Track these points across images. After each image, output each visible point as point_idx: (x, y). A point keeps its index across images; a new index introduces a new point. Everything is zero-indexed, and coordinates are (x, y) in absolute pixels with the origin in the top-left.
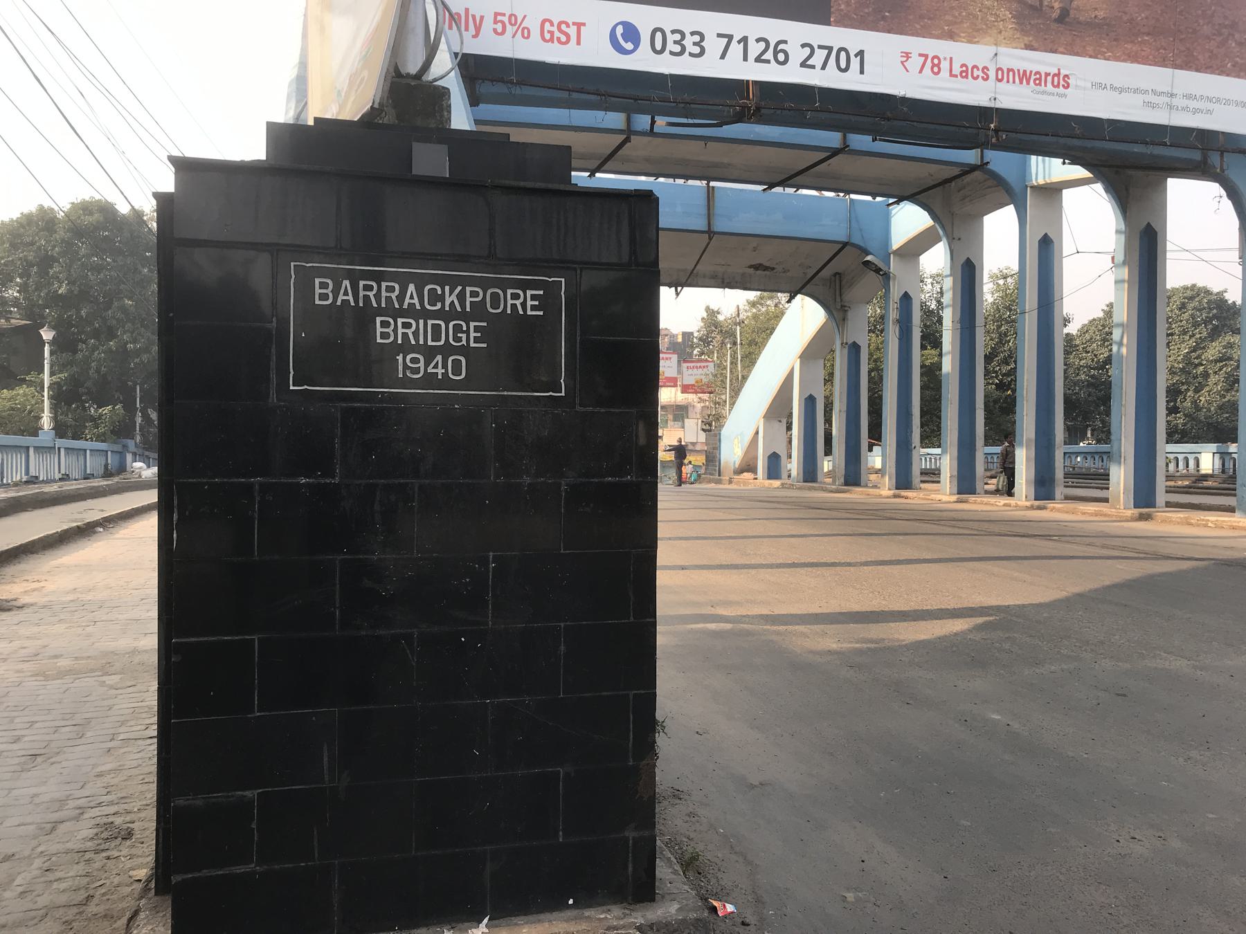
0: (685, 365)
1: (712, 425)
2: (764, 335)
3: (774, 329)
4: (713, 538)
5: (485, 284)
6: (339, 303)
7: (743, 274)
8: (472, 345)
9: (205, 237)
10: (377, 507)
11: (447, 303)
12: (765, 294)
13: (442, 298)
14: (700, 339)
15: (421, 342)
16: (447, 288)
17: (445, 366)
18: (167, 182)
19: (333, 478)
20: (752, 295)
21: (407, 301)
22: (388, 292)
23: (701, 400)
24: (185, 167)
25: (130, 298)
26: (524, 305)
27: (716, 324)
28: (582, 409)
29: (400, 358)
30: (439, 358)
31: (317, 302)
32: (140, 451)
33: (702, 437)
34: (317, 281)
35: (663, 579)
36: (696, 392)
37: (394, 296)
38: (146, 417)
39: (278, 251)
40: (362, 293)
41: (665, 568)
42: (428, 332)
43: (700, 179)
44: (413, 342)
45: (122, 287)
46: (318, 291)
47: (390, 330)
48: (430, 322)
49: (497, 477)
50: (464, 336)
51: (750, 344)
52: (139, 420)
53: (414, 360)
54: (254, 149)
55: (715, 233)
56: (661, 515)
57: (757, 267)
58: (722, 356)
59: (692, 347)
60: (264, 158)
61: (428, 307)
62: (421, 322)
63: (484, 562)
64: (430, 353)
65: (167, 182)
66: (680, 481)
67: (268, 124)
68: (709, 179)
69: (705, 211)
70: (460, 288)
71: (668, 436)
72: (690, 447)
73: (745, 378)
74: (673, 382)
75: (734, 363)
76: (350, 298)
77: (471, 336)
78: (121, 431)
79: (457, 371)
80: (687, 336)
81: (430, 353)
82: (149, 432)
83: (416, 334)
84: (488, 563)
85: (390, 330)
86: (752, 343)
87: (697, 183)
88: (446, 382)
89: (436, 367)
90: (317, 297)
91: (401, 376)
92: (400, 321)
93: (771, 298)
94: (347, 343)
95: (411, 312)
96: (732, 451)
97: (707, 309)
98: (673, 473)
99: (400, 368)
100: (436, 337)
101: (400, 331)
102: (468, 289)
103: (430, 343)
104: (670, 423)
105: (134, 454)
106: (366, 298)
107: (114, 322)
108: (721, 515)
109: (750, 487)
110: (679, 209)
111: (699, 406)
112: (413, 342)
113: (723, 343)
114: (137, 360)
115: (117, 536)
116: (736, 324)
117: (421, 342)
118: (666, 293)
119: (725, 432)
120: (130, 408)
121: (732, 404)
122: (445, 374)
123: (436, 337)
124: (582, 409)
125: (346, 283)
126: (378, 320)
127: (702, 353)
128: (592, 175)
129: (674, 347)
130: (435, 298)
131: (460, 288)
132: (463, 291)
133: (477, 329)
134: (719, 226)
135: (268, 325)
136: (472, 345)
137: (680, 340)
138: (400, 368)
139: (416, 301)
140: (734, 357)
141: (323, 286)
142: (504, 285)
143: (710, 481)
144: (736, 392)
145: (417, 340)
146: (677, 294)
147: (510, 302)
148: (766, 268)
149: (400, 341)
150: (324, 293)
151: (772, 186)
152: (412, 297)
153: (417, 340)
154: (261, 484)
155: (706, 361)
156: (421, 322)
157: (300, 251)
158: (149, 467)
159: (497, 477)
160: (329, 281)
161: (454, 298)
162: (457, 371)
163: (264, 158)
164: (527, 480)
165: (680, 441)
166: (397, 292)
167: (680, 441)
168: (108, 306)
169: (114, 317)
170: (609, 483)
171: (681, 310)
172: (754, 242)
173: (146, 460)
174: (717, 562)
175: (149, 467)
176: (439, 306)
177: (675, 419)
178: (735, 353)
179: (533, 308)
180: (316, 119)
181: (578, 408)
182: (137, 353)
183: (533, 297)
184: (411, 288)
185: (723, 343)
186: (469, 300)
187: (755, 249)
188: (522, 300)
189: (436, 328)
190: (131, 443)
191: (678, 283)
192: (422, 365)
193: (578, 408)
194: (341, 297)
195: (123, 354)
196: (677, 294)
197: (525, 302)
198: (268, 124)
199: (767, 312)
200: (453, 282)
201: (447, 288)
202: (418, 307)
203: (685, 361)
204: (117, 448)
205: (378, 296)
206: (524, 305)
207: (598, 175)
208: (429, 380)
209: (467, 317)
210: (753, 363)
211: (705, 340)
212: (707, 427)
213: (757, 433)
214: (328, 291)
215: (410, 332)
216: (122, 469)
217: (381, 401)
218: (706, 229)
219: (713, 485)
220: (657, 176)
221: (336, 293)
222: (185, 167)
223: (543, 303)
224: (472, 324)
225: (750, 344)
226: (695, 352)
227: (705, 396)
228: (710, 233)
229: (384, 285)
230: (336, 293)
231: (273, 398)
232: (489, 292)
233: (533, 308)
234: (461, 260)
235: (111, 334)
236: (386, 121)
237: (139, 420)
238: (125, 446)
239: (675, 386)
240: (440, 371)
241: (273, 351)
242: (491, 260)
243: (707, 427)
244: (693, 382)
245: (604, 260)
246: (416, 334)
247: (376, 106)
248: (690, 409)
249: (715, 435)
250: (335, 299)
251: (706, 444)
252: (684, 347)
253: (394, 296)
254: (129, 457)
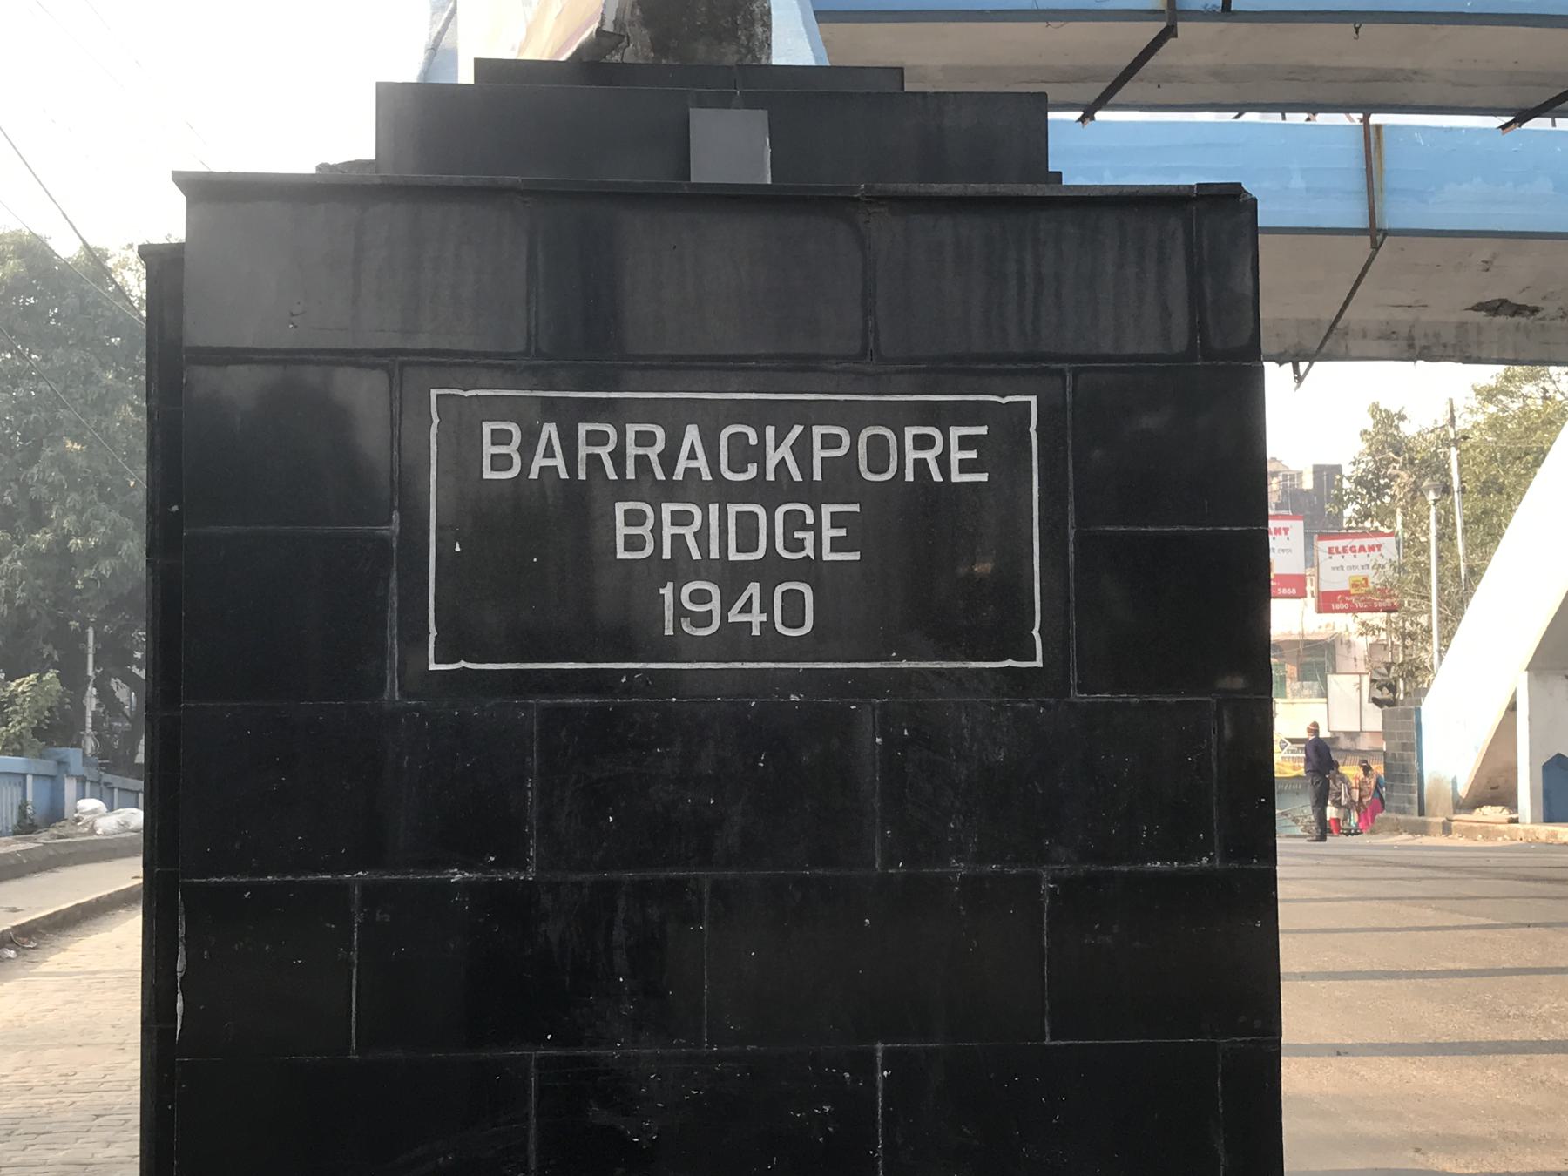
0: (1323, 545)
1: (1399, 689)
2: (1518, 468)
3: (1540, 456)
4: (1411, 975)
5: (853, 418)
6: (534, 475)
7: (1462, 325)
8: (828, 556)
9: (248, 343)
10: (619, 935)
11: (772, 461)
12: (1518, 369)
13: (759, 454)
14: (1360, 482)
15: (714, 555)
16: (770, 431)
17: (766, 607)
18: (169, 222)
19: (523, 869)
20: (1488, 374)
21: (683, 463)
22: (642, 443)
23: (1367, 629)
24: (205, 191)
25: (76, 439)
26: (944, 460)
27: (1398, 445)
28: (1085, 698)
29: (667, 592)
30: (754, 589)
31: (488, 474)
32: (93, 774)
33: (1374, 719)
34: (487, 428)
35: (1297, 1078)
36: (1353, 610)
37: (653, 453)
38: (106, 695)
39: (398, 364)
40: (583, 451)
41: (1285, 932)
42: (729, 524)
43: (1346, 108)
44: (696, 556)
45: (61, 413)
46: (489, 450)
47: (645, 531)
48: (733, 509)
49: (890, 861)
50: (808, 537)
51: (1485, 490)
52: (91, 703)
53: (700, 597)
54: (353, 139)
55: (1386, 233)
56: (1287, 916)
57: (1495, 308)
58: (1415, 522)
59: (1340, 501)
60: (369, 153)
61: (729, 475)
62: (714, 509)
63: (864, 1065)
64: (732, 579)
65: (169, 222)
66: (1324, 830)
67: (378, 84)
68: (1367, 109)
69: (1359, 183)
70: (798, 429)
71: (1293, 717)
72: (1344, 743)
73: (1475, 573)
74: (1297, 586)
75: (1446, 537)
76: (559, 462)
77: (826, 535)
78: (55, 730)
79: (793, 619)
80: (1326, 474)
81: (732, 579)
82: (111, 730)
83: (702, 536)
84: (873, 1072)
85: (645, 531)
86: (1491, 487)
87: (1340, 119)
88: (770, 644)
89: (747, 608)
90: (487, 462)
91: (669, 632)
92: (667, 509)
93: (1531, 378)
94: (544, 553)
95: (691, 488)
96: (1450, 754)
97: (1375, 409)
98: (1306, 810)
99: (669, 614)
100: (747, 544)
101: (668, 531)
102: (818, 431)
103: (733, 556)
104: (1292, 685)
105: (82, 780)
106: (594, 460)
107: (44, 490)
108: (1429, 916)
109: (1499, 842)
110: (1297, 183)
111: (1362, 644)
112: (696, 556)
113: (1416, 491)
114: (89, 573)
115: (44, 968)
116: (1447, 443)
117: (714, 555)
118: (1276, 376)
119: (1430, 709)
120: (73, 679)
121: (1447, 637)
122: (768, 626)
123: (747, 544)
124: (1085, 698)
125: (550, 430)
126: (620, 508)
127: (1365, 515)
128: (1088, 115)
129: (1297, 502)
130: (744, 454)
131: (798, 429)
132: (806, 438)
133: (837, 521)
134: (1396, 215)
135: (383, 531)
136: (828, 556)
137: (1308, 483)
138: (669, 614)
139: (701, 463)
140: (1445, 522)
141: (501, 437)
142: (897, 418)
143: (1397, 829)
144: (1454, 609)
145: (704, 547)
146: (1299, 379)
147: (912, 455)
148: (1518, 310)
149: (667, 555)
150: (503, 455)
151: (1522, 116)
152: (692, 455)
153: (704, 547)
154: (365, 886)
155: (1376, 533)
156: (714, 509)
157: (446, 362)
158: (111, 809)
159: (890, 861)
160: (513, 428)
161: (785, 451)
162: (793, 619)
163: (369, 153)
164: (959, 868)
165: (1314, 729)
166: (660, 445)
167: (1314, 729)
168: (33, 457)
169: (43, 482)
170: (1157, 874)
171: (1313, 418)
172: (1485, 249)
173: (105, 792)
174: (1424, 1037)
175: (111, 809)
176: (753, 470)
177: (1303, 676)
178: (1449, 512)
179: (965, 466)
180: (480, 64)
181: (1076, 696)
182: (91, 557)
183: (965, 443)
184: (692, 434)
185: (1416, 491)
186: (819, 454)
187: (1487, 266)
188: (938, 449)
189: (747, 524)
190: (74, 756)
191: (1296, 356)
192: (715, 605)
193: (1076, 696)
194: (539, 462)
195: (62, 560)
196: (1299, 379)
197: (948, 454)
198: (378, 84)
199: (1525, 413)
200: (781, 417)
201: (770, 431)
202: (706, 476)
203: (1322, 537)
204: (47, 766)
205: (618, 457)
206: (944, 460)
207: (1100, 115)
208: (733, 640)
209: (814, 495)
210: (1495, 535)
211: (1372, 485)
212: (1385, 694)
213: (1512, 707)
214: (512, 449)
215: (688, 533)
216: (55, 814)
217: (628, 690)
218: (1363, 223)
219: (1404, 839)
220: (1241, 108)
221: (527, 450)
222: (205, 191)
223: (986, 453)
224: (827, 510)
225: (1485, 490)
226: (1348, 513)
227: (1378, 619)
228: (1376, 234)
229: (632, 430)
230: (527, 450)
231: (392, 691)
232: (865, 434)
233: (965, 466)
234: (800, 367)
235: (38, 519)
236: (629, 57)
237: (91, 703)
238: (62, 764)
239: (1301, 594)
240: (756, 618)
241: (393, 584)
242: (868, 362)
243: (1385, 694)
244: (1346, 586)
245: (1130, 349)
246: (702, 536)
247: (609, 28)
248: (1341, 650)
249: (1407, 714)
250: (526, 467)
251: (1386, 734)
252: (1321, 507)
253: (653, 453)
254: (70, 787)
